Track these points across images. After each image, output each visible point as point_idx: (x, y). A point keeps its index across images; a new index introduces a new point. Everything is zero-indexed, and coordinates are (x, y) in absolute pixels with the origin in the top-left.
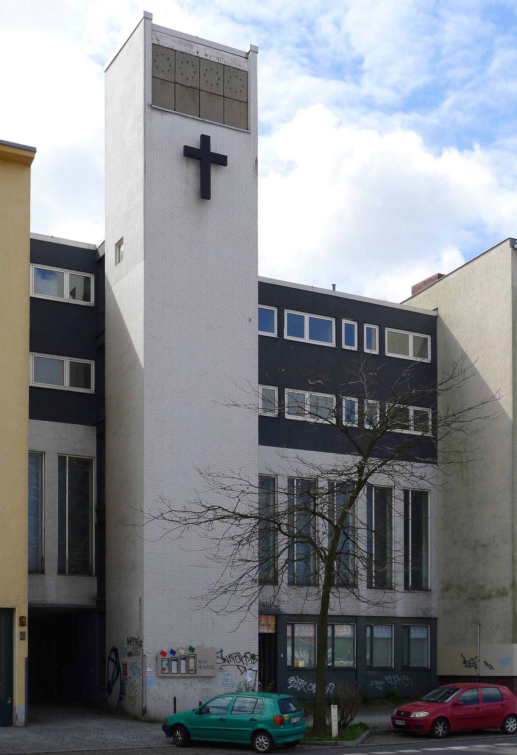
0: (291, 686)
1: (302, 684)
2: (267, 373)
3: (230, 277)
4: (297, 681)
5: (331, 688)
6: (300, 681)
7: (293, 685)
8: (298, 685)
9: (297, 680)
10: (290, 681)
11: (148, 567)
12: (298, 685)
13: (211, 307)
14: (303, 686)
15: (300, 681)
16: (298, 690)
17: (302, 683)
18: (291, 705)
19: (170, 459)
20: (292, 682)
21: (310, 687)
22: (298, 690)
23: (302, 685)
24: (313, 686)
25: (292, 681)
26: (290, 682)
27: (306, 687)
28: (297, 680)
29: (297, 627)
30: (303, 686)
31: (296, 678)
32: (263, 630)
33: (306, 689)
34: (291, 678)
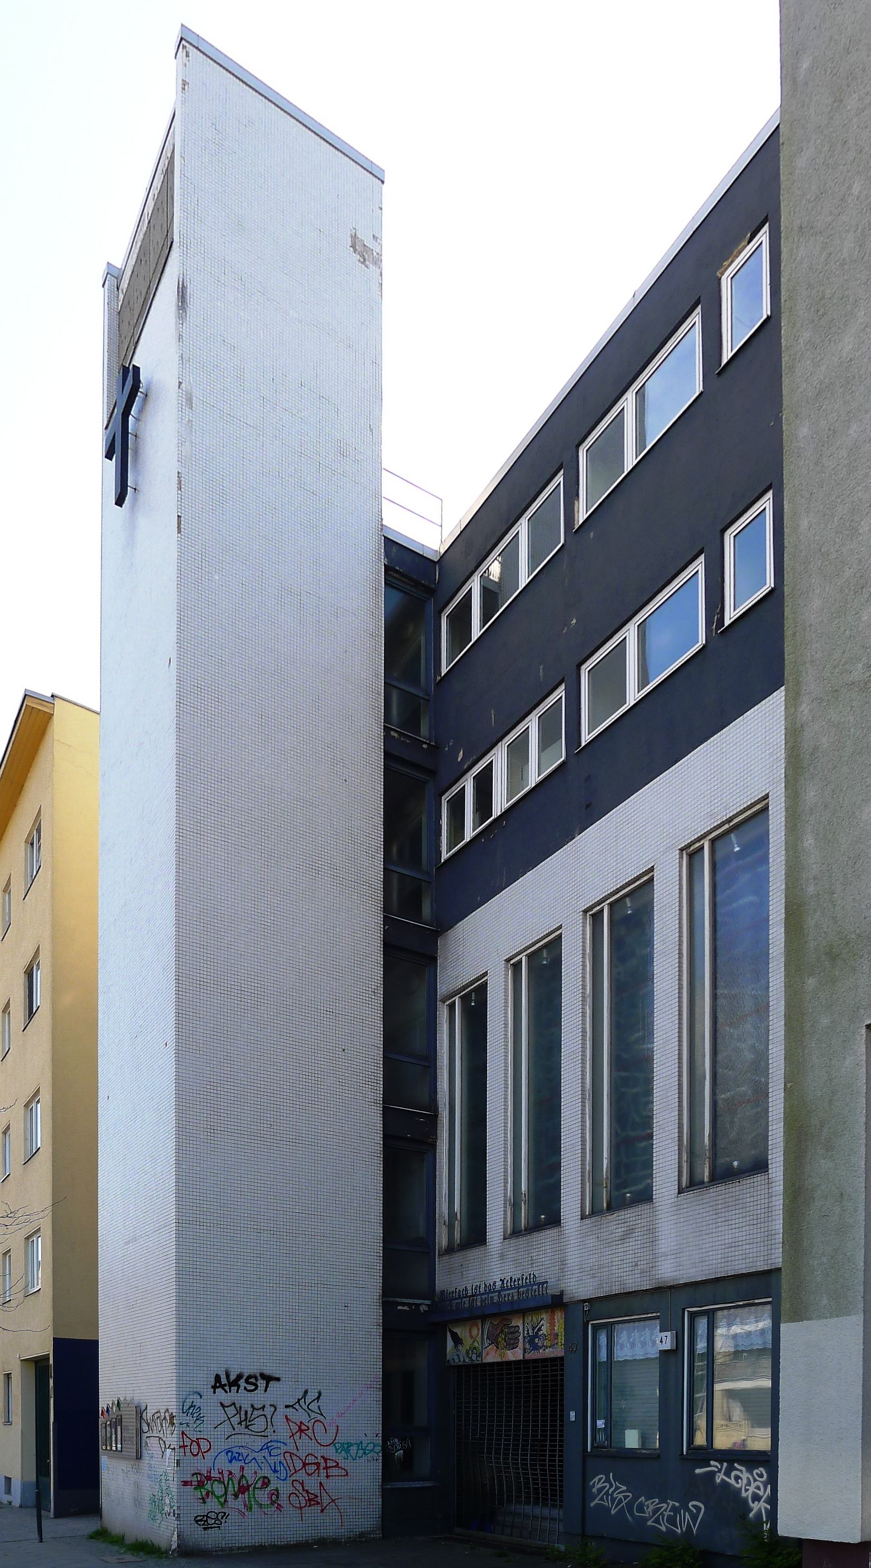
0: (596, 1501)
1: (621, 1496)
2: (698, 1471)
3: (259, 1192)
4: (610, 1488)
5: (694, 1518)
6: (617, 1488)
7: (602, 1499)
8: (613, 1500)
9: (611, 1486)
10: (594, 1486)
11: (275, 1194)
12: (613, 1500)
13: (188, 1116)
14: (624, 1502)
15: (617, 1488)
16: (613, 1512)
17: (621, 1492)
18: (592, 1505)
19: (269, 1115)
20: (600, 1490)
21: (641, 1509)
22: (613, 1512)
23: (620, 1501)
24: (648, 1507)
25: (599, 1486)
26: (594, 1490)
27: (630, 1505)
28: (611, 1486)
29: (624, 1336)
30: (624, 1502)
31: (608, 1480)
32: (544, 1350)
33: (632, 1514)
34: (596, 1479)
